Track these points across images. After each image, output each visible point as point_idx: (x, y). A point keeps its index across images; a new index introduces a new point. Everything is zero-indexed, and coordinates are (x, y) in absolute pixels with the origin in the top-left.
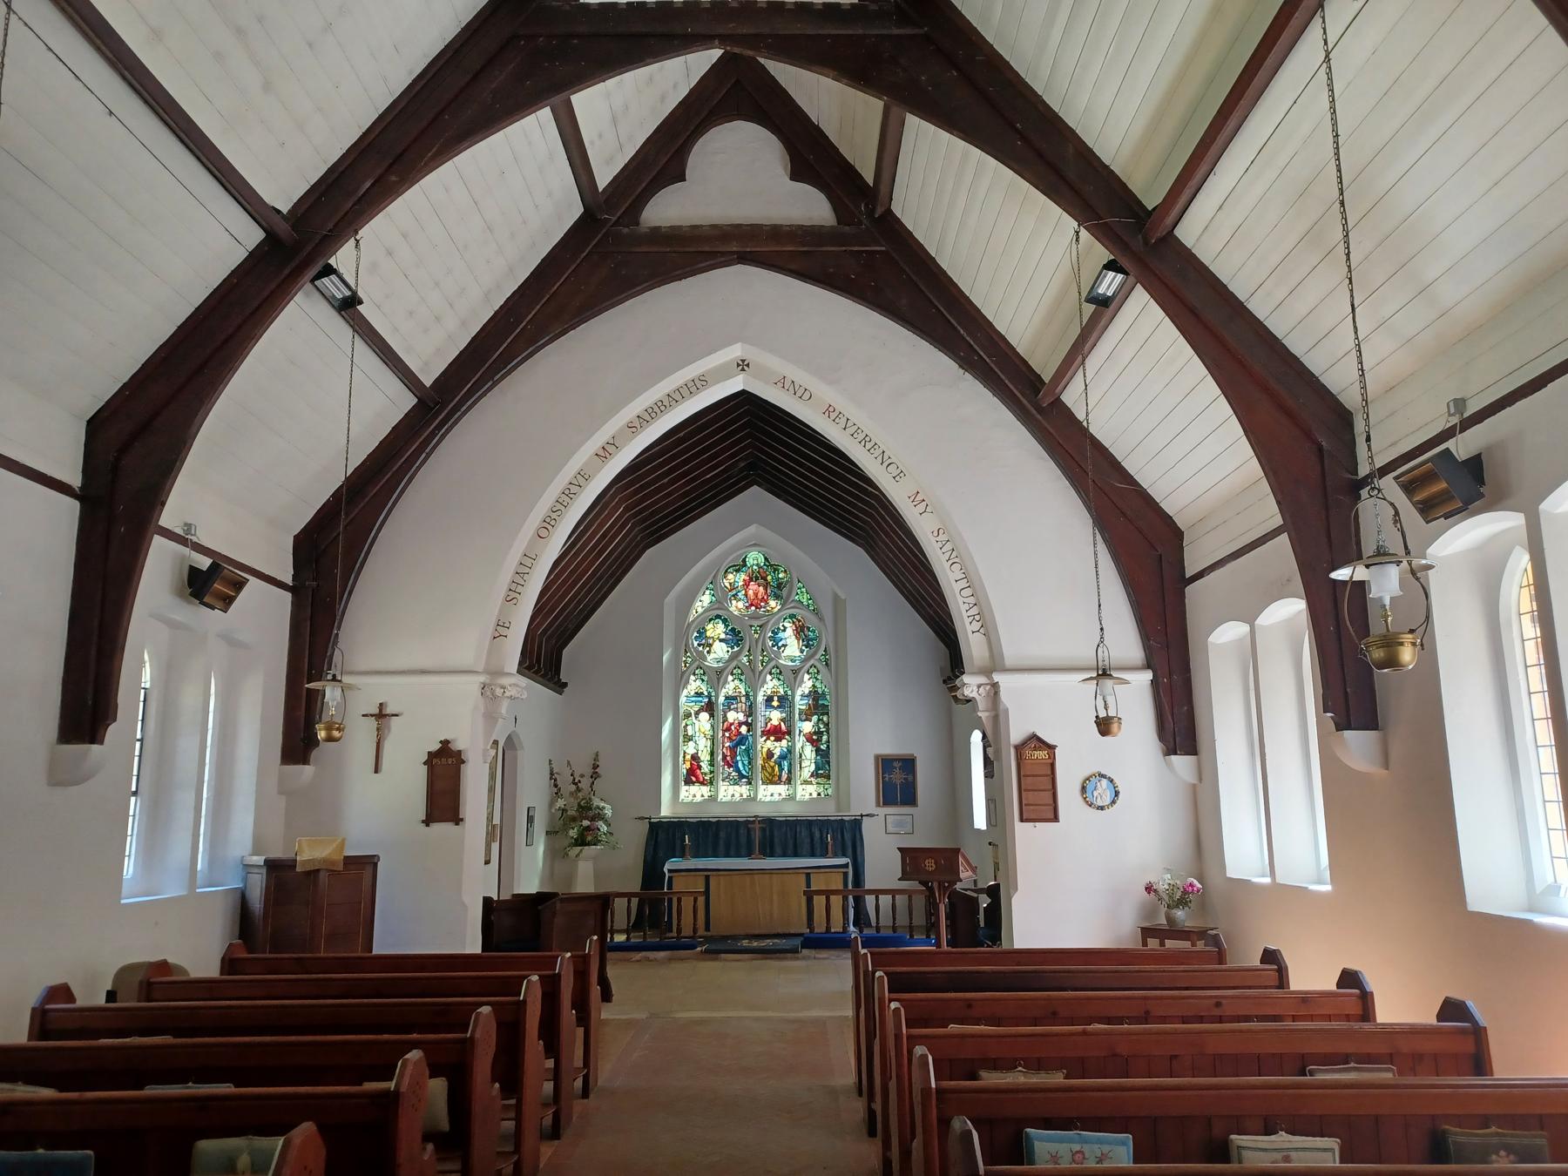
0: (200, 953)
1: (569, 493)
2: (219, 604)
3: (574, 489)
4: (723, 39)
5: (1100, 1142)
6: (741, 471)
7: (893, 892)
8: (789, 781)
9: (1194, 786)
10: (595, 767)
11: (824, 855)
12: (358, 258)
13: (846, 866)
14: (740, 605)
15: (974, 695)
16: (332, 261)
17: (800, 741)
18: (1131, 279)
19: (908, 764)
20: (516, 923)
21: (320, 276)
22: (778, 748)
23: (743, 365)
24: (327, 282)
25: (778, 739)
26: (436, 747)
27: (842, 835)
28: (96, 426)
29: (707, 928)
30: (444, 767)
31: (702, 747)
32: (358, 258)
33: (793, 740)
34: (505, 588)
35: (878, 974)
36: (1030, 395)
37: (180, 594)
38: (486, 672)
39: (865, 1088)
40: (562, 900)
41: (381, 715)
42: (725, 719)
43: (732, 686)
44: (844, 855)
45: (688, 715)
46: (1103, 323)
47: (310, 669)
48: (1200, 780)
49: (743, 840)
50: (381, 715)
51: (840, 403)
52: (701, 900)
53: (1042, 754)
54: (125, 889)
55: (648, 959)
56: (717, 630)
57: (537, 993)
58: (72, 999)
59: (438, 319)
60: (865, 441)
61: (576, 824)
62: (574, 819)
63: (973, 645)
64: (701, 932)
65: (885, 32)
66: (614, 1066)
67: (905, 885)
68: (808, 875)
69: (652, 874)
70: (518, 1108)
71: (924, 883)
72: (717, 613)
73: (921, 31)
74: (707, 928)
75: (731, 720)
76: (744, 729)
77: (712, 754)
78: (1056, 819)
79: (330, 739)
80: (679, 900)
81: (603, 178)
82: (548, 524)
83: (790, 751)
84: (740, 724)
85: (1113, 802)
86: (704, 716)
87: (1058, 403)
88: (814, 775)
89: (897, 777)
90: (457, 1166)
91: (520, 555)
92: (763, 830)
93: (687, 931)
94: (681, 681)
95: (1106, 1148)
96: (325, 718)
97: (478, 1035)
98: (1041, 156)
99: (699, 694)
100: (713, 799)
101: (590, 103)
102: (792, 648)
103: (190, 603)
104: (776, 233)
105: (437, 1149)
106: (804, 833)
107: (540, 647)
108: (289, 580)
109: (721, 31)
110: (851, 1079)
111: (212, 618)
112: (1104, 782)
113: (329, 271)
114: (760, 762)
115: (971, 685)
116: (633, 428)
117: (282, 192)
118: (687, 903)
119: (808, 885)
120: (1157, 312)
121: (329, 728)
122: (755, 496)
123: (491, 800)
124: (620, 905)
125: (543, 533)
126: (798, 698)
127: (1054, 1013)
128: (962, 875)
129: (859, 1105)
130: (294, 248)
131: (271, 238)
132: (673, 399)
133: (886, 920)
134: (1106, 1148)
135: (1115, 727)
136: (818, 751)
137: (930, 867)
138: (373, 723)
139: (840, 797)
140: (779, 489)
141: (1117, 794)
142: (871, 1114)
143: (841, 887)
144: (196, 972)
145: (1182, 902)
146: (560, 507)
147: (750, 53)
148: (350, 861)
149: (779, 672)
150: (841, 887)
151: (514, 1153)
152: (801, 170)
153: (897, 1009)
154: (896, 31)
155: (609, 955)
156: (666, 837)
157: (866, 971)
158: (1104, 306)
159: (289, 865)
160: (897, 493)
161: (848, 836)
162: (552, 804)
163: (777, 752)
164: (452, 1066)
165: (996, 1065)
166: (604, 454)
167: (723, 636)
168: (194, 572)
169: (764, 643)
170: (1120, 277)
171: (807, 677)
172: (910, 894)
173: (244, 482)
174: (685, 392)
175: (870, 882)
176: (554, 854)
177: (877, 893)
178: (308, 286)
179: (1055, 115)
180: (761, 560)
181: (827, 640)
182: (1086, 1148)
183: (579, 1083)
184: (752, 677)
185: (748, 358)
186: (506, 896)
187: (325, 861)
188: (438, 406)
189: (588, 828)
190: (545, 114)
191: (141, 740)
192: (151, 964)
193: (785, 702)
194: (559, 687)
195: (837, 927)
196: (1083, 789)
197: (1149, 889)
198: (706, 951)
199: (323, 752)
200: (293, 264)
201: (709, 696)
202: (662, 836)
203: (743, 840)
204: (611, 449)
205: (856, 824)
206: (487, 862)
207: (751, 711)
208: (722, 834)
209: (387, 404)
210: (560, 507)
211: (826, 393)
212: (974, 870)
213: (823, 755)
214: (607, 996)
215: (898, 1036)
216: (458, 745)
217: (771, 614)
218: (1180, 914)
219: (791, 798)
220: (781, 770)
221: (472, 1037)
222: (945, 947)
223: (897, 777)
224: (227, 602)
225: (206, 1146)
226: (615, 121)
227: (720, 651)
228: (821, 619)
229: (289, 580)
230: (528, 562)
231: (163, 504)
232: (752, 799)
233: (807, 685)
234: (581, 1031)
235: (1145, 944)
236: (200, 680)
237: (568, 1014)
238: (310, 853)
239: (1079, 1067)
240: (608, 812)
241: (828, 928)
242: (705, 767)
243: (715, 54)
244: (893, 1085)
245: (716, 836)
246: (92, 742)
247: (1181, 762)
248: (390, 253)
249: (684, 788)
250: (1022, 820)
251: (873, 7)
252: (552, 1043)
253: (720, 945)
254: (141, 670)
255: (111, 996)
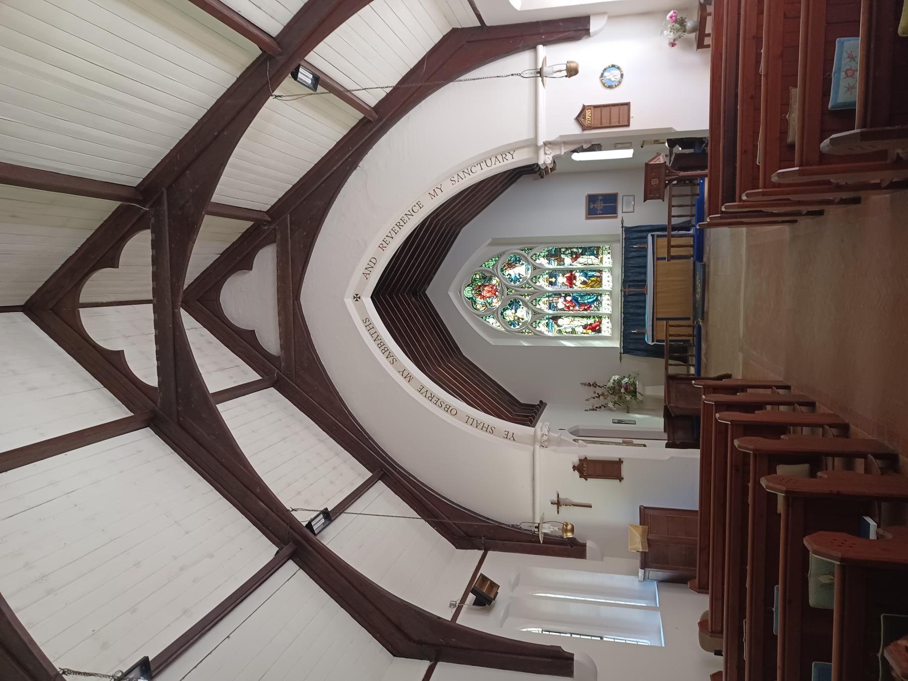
0: (695, 606)
1: (431, 397)
2: (495, 590)
3: (429, 395)
4: (174, 307)
5: (840, 59)
6: (417, 300)
7: (670, 206)
8: (600, 271)
9: (609, 18)
10: (589, 385)
11: (646, 249)
12: (303, 510)
13: (653, 236)
14: (495, 301)
15: (551, 157)
16: (304, 524)
17: (577, 265)
18: (302, 63)
19: (592, 199)
20: (681, 428)
21: (312, 531)
22: (580, 278)
23: (357, 298)
24: (316, 527)
25: (575, 278)
26: (577, 473)
27: (634, 239)
28: (396, 652)
29: (688, 319)
30: (587, 469)
31: (579, 323)
32: (303, 510)
33: (575, 269)
34: (486, 434)
35: (723, 209)
36: (374, 123)
37: (489, 611)
38: (533, 444)
39: (791, 219)
40: (669, 402)
41: (558, 503)
42: (562, 309)
43: (543, 306)
44: (646, 237)
45: (560, 331)
46: (328, 80)
47: (531, 541)
48: (605, 13)
49: (636, 298)
50: (558, 503)
51: (378, 240)
52: (671, 322)
53: (588, 113)
54: (658, 644)
55: (706, 354)
56: (510, 314)
57: (726, 414)
58: (720, 673)
59: (334, 468)
60: (399, 225)
61: (623, 396)
62: (620, 397)
63: (521, 158)
64: (690, 322)
65: (166, 213)
66: (772, 372)
67: (667, 199)
68: (658, 259)
69: (655, 352)
70: (795, 425)
71: (666, 185)
72: (499, 315)
73: (165, 192)
74: (688, 319)
75: (563, 306)
76: (569, 298)
77: (583, 317)
78: (628, 104)
79: (572, 530)
80: (671, 335)
81: (254, 376)
82: (448, 409)
83: (582, 271)
84: (565, 300)
85: (618, 68)
86: (560, 321)
87: (377, 108)
88: (597, 256)
89: (599, 205)
90: (830, 459)
91: (465, 425)
92: (629, 286)
93: (689, 331)
94: (539, 335)
95: (845, 55)
96: (560, 533)
97: (752, 447)
98: (233, 119)
99: (547, 325)
100: (610, 316)
101: (214, 383)
102: (520, 270)
103: (494, 606)
104: (281, 278)
105: (820, 470)
106: (632, 262)
107: (519, 416)
108: (481, 552)
109: (170, 308)
110: (786, 228)
111: (503, 594)
112: (606, 74)
113: (309, 526)
114: (588, 289)
115: (545, 159)
116: (394, 361)
117: (267, 550)
118: (672, 331)
119: (664, 259)
120: (321, 47)
121: (566, 531)
122: (432, 292)
123: (608, 443)
124: (672, 370)
125: (454, 412)
126: (551, 267)
127: (752, 98)
128: (662, 162)
129: (803, 222)
130: (297, 544)
131: (293, 556)
132: (377, 338)
133: (686, 211)
134: (845, 55)
135: (573, 65)
136: (582, 254)
137: (655, 181)
138: (562, 508)
139: (610, 240)
140: (428, 278)
141: (613, 66)
142: (810, 213)
143: (666, 239)
144: (707, 607)
145: (682, 23)
146: (438, 402)
147: (181, 292)
148: (642, 523)
149: (535, 278)
150: (666, 239)
151: (823, 428)
152: (246, 264)
153: (747, 195)
154: (166, 207)
155: (703, 375)
156: (632, 342)
157: (720, 218)
158: (319, 80)
159: (644, 555)
160: (430, 206)
161: (635, 235)
162: (611, 410)
163: (583, 279)
164: (773, 460)
165: (784, 132)
166: (409, 378)
167: (513, 311)
168: (477, 603)
169: (518, 287)
170: (301, 70)
171: (538, 261)
172: (671, 196)
173: (424, 572)
174: (372, 331)
175: (665, 222)
176: (640, 410)
177: (670, 216)
178: (318, 537)
179: (209, 111)
180: (468, 288)
181: (516, 249)
182: (844, 68)
183: (781, 391)
184: (538, 293)
185: (353, 294)
186: (665, 436)
187: (642, 536)
188: (383, 469)
189: (626, 389)
190: (220, 407)
191: (571, 634)
192: (701, 631)
193: (553, 274)
194: (542, 405)
195: (690, 241)
196: (610, 87)
197: (673, 45)
198: (703, 319)
199: (578, 535)
200: (304, 543)
201: (548, 319)
202: (631, 346)
203: (636, 298)
204: (405, 374)
205: (628, 230)
206: (645, 446)
207: (558, 294)
208: (632, 311)
209: (382, 497)
210: (438, 402)
211: (372, 250)
212: (659, 154)
213: (586, 251)
214: (728, 376)
215: (763, 194)
216: (576, 461)
217: (501, 282)
218: (689, 24)
219: (611, 270)
220: (593, 276)
221: (754, 450)
222: (706, 171)
223: (599, 205)
224: (494, 586)
225: (812, 601)
226: (223, 369)
227: (522, 312)
228: (504, 253)
229: (481, 552)
230: (470, 421)
231: (439, 618)
232: (611, 293)
233: (543, 261)
234: (749, 390)
235: (708, 46)
236: (538, 603)
237: (740, 397)
238: (637, 543)
239: (789, 79)
240: (616, 377)
241: (691, 246)
242: (591, 321)
243: (183, 312)
244: (794, 198)
245: (632, 314)
246: (573, 659)
247: (594, 26)
248: (299, 493)
249: (603, 334)
250: (628, 125)
251: (153, 220)
252: (760, 406)
253: (699, 310)
254: (532, 633)
255: (718, 653)
